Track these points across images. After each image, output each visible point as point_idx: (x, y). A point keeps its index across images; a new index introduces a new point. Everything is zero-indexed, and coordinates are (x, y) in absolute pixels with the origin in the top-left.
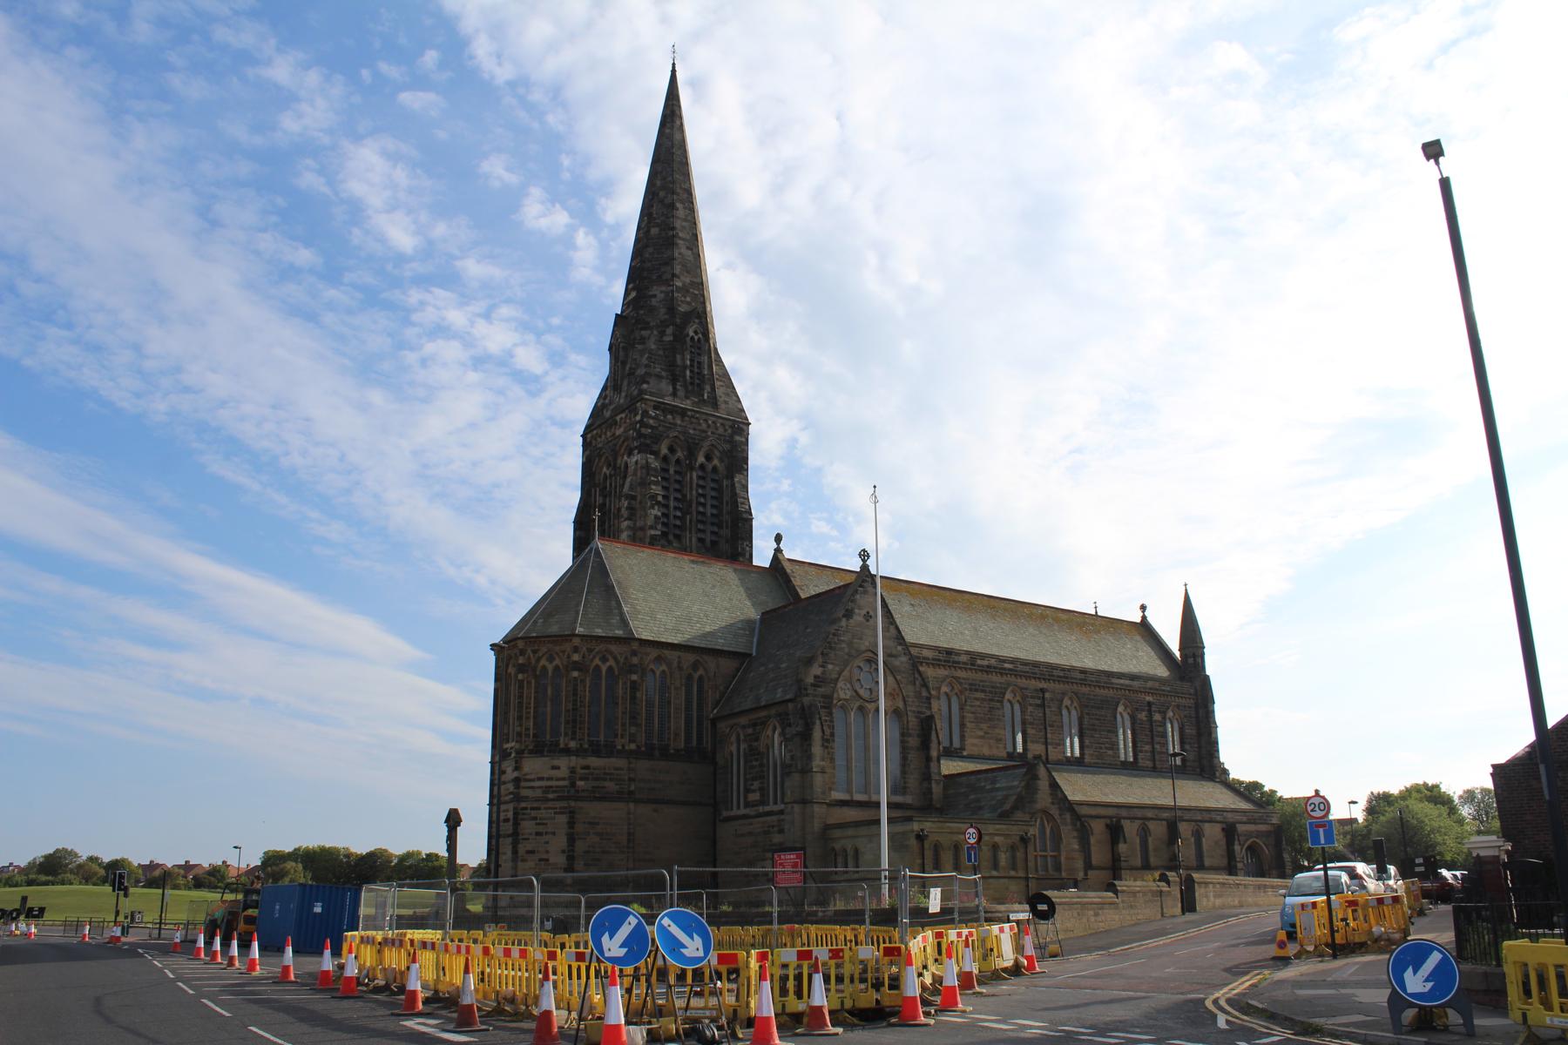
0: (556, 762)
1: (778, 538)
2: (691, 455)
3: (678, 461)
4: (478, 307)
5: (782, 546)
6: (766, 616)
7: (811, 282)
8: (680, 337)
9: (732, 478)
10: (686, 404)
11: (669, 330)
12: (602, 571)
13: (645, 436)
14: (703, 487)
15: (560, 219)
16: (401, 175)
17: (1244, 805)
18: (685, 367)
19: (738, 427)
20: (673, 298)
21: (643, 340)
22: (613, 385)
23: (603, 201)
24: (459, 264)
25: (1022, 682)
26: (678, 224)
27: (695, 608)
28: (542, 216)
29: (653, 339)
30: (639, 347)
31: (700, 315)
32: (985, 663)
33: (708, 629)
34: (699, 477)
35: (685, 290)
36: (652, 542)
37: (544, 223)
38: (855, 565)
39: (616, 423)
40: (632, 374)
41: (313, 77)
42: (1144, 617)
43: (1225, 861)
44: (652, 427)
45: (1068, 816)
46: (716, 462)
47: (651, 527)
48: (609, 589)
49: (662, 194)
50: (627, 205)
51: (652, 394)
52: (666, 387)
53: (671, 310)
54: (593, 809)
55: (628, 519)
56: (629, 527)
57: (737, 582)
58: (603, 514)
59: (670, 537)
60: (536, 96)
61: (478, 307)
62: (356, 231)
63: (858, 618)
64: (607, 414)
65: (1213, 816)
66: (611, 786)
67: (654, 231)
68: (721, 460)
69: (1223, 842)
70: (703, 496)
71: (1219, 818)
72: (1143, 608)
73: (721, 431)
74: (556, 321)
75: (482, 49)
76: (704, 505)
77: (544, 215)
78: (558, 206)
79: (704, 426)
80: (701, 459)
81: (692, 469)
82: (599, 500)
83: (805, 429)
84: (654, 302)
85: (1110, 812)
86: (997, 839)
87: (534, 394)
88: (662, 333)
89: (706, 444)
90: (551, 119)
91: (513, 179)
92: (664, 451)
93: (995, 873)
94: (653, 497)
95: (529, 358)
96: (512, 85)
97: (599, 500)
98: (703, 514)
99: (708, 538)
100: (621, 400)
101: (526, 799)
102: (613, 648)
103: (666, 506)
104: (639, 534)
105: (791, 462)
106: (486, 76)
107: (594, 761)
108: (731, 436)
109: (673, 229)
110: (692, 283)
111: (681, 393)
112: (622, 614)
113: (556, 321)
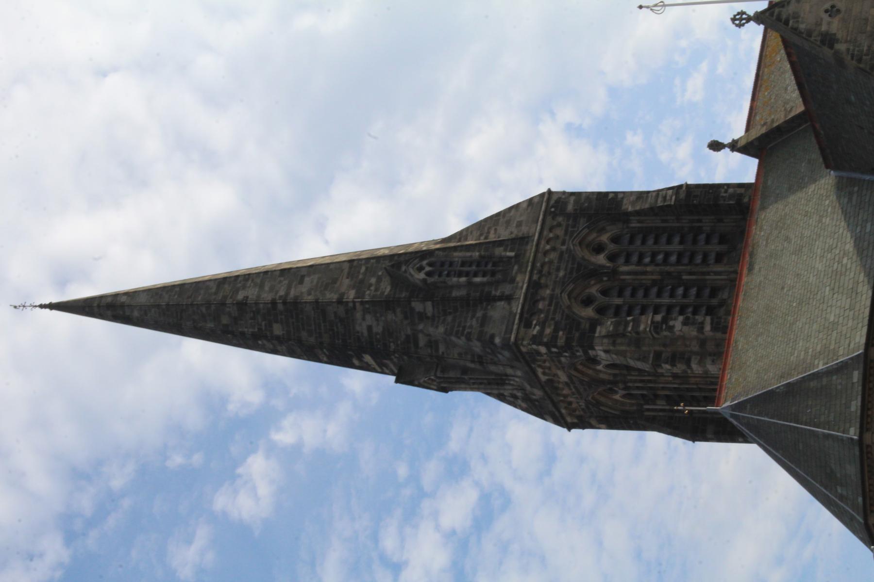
1: (716, 146)
2: (595, 273)
3: (604, 292)
5: (727, 140)
6: (832, 159)
7: (346, 109)
8: (426, 292)
9: (627, 214)
10: (523, 281)
11: (418, 306)
12: (766, 400)
13: (568, 341)
14: (641, 256)
15: (258, 466)
18: (470, 284)
19: (554, 207)
20: (373, 303)
21: (432, 344)
22: (497, 387)
23: (231, 407)
26: (267, 297)
27: (819, 266)
28: (255, 491)
29: (431, 330)
30: (442, 349)
31: (395, 264)
33: (850, 247)
34: (627, 262)
35: (360, 286)
36: (723, 328)
37: (264, 490)
38: (755, 33)
39: (550, 382)
40: (480, 360)
44: (556, 331)
46: (605, 238)
47: (701, 329)
48: (792, 390)
49: (225, 320)
50: (236, 370)
51: (509, 331)
52: (498, 310)
53: (388, 304)
55: (688, 362)
56: (701, 363)
57: (780, 205)
58: (681, 399)
59: (715, 304)
60: (86, 503)
63: (835, 26)
64: (538, 393)
67: (278, 330)
68: (602, 231)
70: (654, 255)
73: (560, 232)
74: (402, 471)
76: (667, 255)
77: (254, 489)
78: (240, 471)
79: (553, 256)
80: (601, 259)
81: (614, 273)
82: (661, 404)
83: (552, 114)
84: (378, 329)
87: (507, 501)
88: (422, 316)
89: (581, 253)
90: (117, 483)
91: (203, 534)
92: (589, 312)
94: (656, 327)
95: (456, 508)
96: (70, 538)
97: (661, 404)
98: (680, 255)
99: (715, 248)
100: (517, 375)
103: (670, 309)
104: (710, 347)
105: (602, 132)
106: (58, 574)
108: (568, 216)
109: (274, 303)
111: (507, 289)
112: (829, 372)
113: (402, 471)
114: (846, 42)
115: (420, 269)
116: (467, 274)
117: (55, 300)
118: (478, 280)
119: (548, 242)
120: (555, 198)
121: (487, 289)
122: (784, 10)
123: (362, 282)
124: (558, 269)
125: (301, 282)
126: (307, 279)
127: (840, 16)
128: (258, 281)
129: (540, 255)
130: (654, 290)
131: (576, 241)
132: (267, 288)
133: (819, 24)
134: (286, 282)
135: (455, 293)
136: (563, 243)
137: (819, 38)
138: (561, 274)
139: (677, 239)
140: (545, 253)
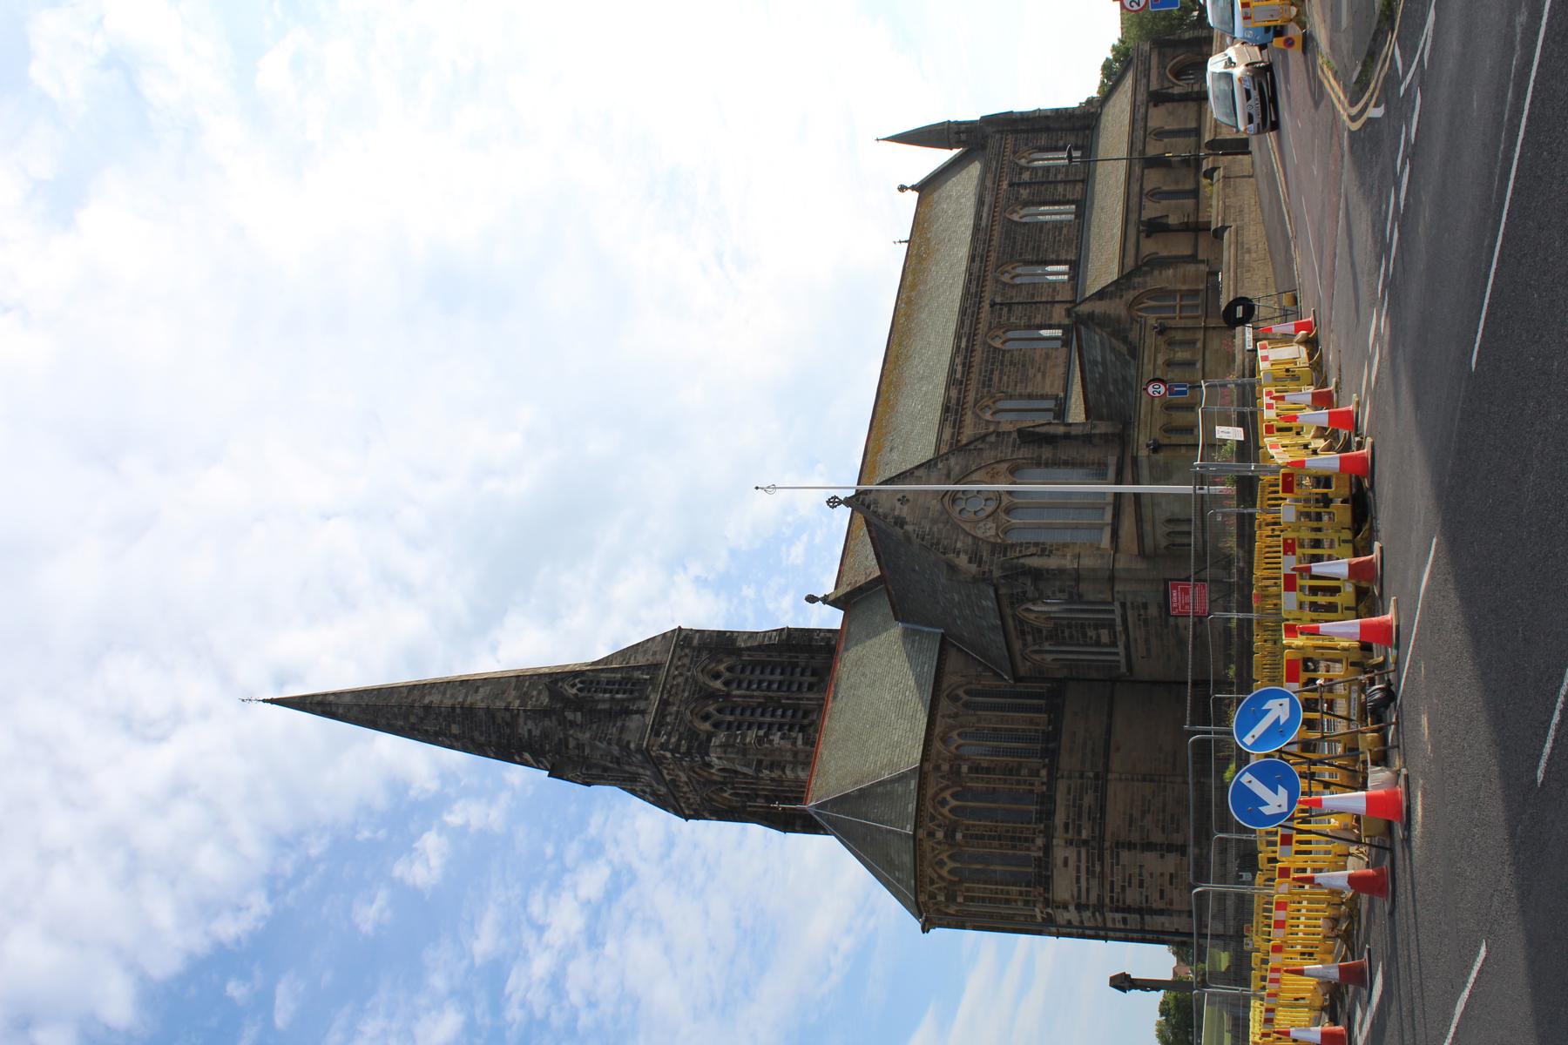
0: (1059, 862)
10: (655, 699)
15: (432, 843)
24: (478, 961)
25: (983, 327)
32: (959, 368)
38: (844, 513)
42: (913, 188)
45: (1136, 280)
46: (722, 667)
54: (1115, 821)
65: (1139, 116)
66: (1088, 799)
68: (720, 661)
69: (1169, 106)
71: (1142, 110)
72: (902, 188)
74: (549, 850)
75: (228, 929)
84: (537, 732)
86: (1160, 361)
91: (382, 896)
93: (1199, 365)
101: (1100, 898)
102: (930, 792)
107: (1060, 818)
111: (642, 705)
113: (549, 850)
115: (573, 686)
123: (526, 693)
125: (477, 691)
133: (893, 509)
135: (600, 706)
139: (778, 671)
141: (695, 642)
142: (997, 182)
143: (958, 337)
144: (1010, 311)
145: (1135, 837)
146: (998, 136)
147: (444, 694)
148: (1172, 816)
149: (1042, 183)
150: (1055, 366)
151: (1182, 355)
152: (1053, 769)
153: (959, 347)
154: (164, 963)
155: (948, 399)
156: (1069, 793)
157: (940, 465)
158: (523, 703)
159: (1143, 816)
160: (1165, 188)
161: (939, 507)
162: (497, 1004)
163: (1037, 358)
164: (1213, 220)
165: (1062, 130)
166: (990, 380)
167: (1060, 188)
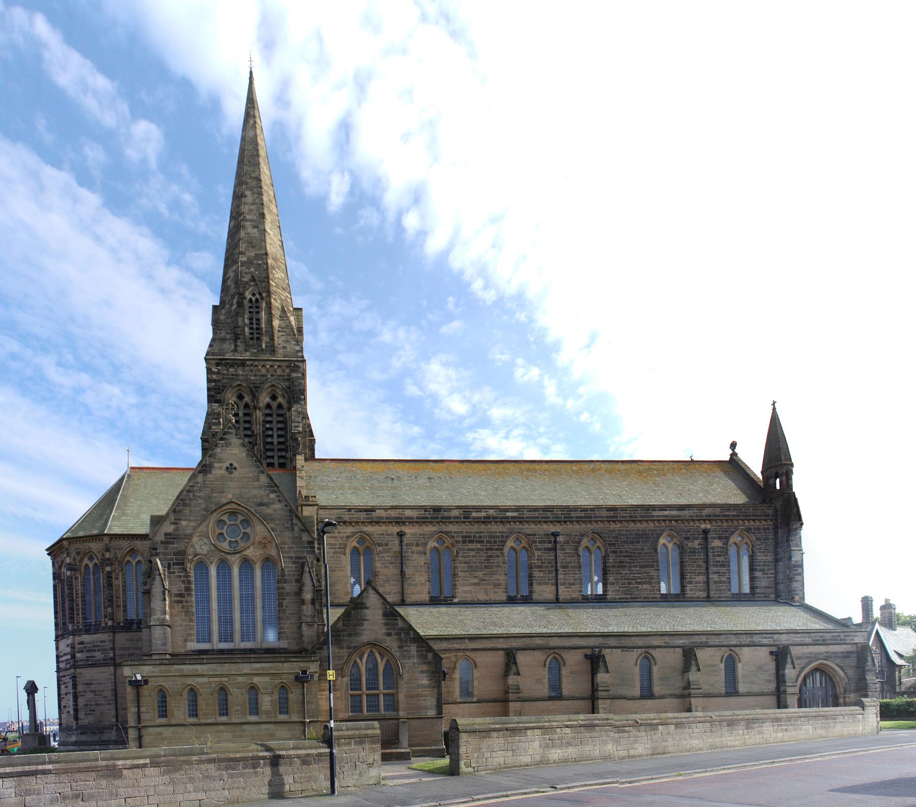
2: (255, 397)
4: (502, 433)
10: (247, 356)
15: (535, 373)
16: (452, 373)
17: (830, 626)
24: (488, 413)
25: (529, 528)
32: (483, 514)
41: (401, 333)
42: (734, 455)
43: (772, 686)
45: (413, 648)
46: (280, 399)
54: (88, 674)
61: (502, 433)
62: (436, 411)
65: (756, 639)
66: (99, 655)
68: (284, 397)
69: (772, 665)
71: (765, 641)
72: (733, 445)
74: (542, 430)
75: (477, 285)
85: (592, 642)
86: (256, 680)
91: (506, 357)
92: (232, 400)
93: (253, 718)
107: (86, 638)
110: (257, 256)
111: (241, 348)
113: (542, 430)
114: (204, 481)
115: (254, 295)
116: (251, 323)
117: (255, 82)
118: (247, 330)
119: (271, 366)
120: (300, 364)
121: (241, 337)
122: (234, 436)
123: (252, 263)
124: (255, 375)
125: (254, 227)
126: (256, 230)
127: (227, 474)
128: (257, 201)
129: (263, 363)
130: (249, 433)
131: (274, 383)
132: (252, 207)
133: (220, 461)
134: (255, 218)
135: (240, 319)
136: (272, 375)
137: (208, 462)
138: (252, 378)
139: (281, 440)
140: (264, 366)
141: (294, 375)
142: (708, 519)
143: (518, 509)
144: (549, 549)
145: (80, 688)
146: (771, 512)
147: (253, 204)
148: (94, 710)
149: (707, 562)
150: (487, 593)
151: (266, 702)
152: (114, 630)
153: (507, 510)
154: (457, 261)
155: (448, 509)
156: (101, 642)
157: (272, 496)
158: (243, 264)
159: (93, 692)
160: (655, 669)
161: (224, 501)
162: (472, 428)
163: (495, 577)
164: (868, 699)
165: (776, 573)
166: (470, 542)
167: (701, 578)
